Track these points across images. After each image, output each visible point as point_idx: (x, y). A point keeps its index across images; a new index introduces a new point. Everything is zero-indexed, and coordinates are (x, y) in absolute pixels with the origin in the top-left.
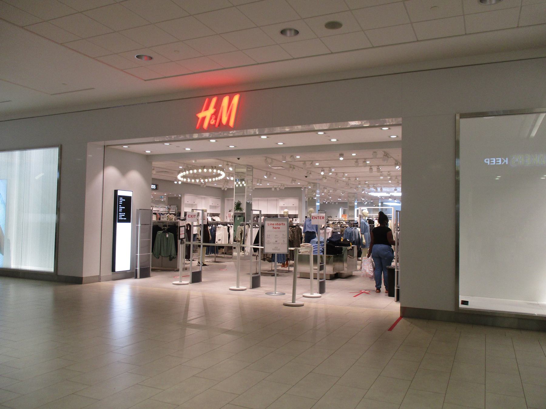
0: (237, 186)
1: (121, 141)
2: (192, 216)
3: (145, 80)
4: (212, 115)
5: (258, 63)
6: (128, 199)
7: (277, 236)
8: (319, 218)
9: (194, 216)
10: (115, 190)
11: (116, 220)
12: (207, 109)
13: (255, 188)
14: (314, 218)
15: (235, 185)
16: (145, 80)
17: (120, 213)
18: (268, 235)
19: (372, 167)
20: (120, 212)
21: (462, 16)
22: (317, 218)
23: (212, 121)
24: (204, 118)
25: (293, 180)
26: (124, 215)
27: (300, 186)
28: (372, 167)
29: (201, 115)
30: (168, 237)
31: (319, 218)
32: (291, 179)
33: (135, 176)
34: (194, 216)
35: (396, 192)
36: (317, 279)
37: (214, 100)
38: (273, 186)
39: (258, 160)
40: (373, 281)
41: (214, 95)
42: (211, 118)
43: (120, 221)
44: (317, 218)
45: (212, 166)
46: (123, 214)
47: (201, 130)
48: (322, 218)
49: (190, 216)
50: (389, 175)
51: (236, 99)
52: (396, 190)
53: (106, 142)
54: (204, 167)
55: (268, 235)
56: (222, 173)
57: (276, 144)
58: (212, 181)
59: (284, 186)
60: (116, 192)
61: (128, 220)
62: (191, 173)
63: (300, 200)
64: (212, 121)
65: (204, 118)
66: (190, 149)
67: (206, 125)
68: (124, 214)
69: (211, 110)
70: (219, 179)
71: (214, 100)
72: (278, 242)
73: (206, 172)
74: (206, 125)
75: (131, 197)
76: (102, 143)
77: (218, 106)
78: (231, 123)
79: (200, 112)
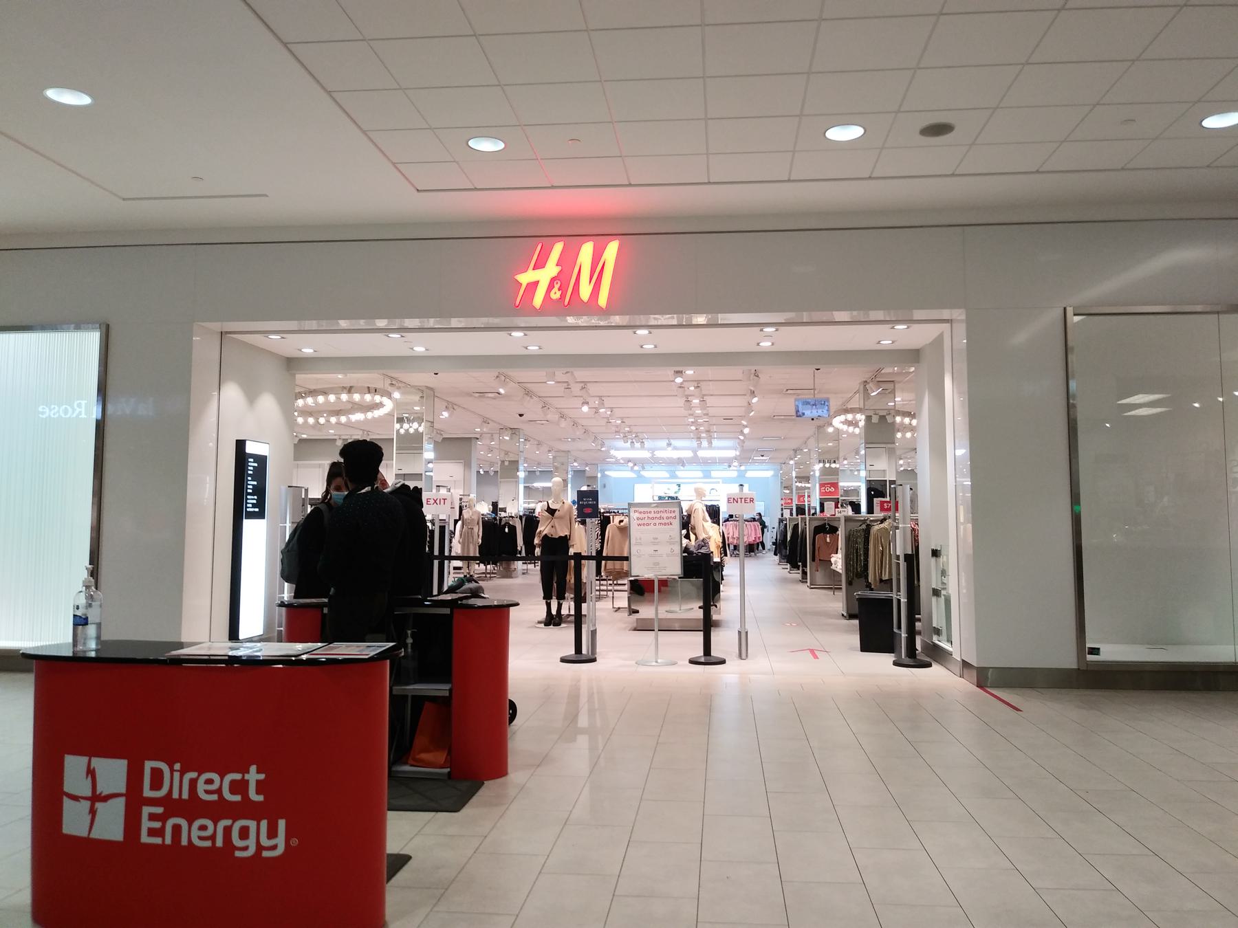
0: (402, 431)
1: (475, 319)
2: (438, 502)
3: (124, 199)
4: (553, 280)
5: (476, 188)
6: (261, 460)
7: (657, 539)
8: (743, 500)
9: (442, 501)
10: (237, 441)
11: (239, 515)
12: (540, 265)
13: (444, 439)
14: (732, 501)
15: (398, 431)
16: (124, 199)
17: (249, 497)
18: (638, 538)
19: (705, 398)
20: (250, 494)
21: (705, 152)
22: (739, 500)
23: (555, 293)
24: (534, 285)
25: (485, 422)
26: (255, 501)
27: (334, 437)
28: (705, 398)
29: (525, 278)
30: (539, 554)
31: (743, 500)
32: (710, 415)
33: (268, 404)
34: (442, 501)
35: (670, 449)
36: (654, 630)
37: (558, 248)
38: (340, 435)
39: (484, 379)
40: (848, 631)
41: (586, 236)
42: (550, 287)
43: (251, 516)
44: (739, 500)
45: (369, 387)
46: (254, 499)
47: (524, 307)
48: (749, 500)
49: (432, 501)
50: (692, 415)
51: (612, 250)
52: (669, 445)
53: (225, 323)
54: (325, 393)
55: (638, 538)
56: (385, 400)
57: (411, 350)
58: (339, 423)
59: (442, 435)
60: (240, 445)
61: (260, 515)
62: (321, 402)
63: (467, 465)
64: (555, 293)
65: (534, 285)
66: (311, 351)
67: (538, 300)
68: (256, 497)
69: (551, 269)
70: (376, 416)
71: (558, 248)
72: (659, 552)
73: (322, 404)
74: (538, 300)
75: (266, 456)
76: (217, 326)
77: (568, 261)
78: (603, 300)
79: (525, 270)
